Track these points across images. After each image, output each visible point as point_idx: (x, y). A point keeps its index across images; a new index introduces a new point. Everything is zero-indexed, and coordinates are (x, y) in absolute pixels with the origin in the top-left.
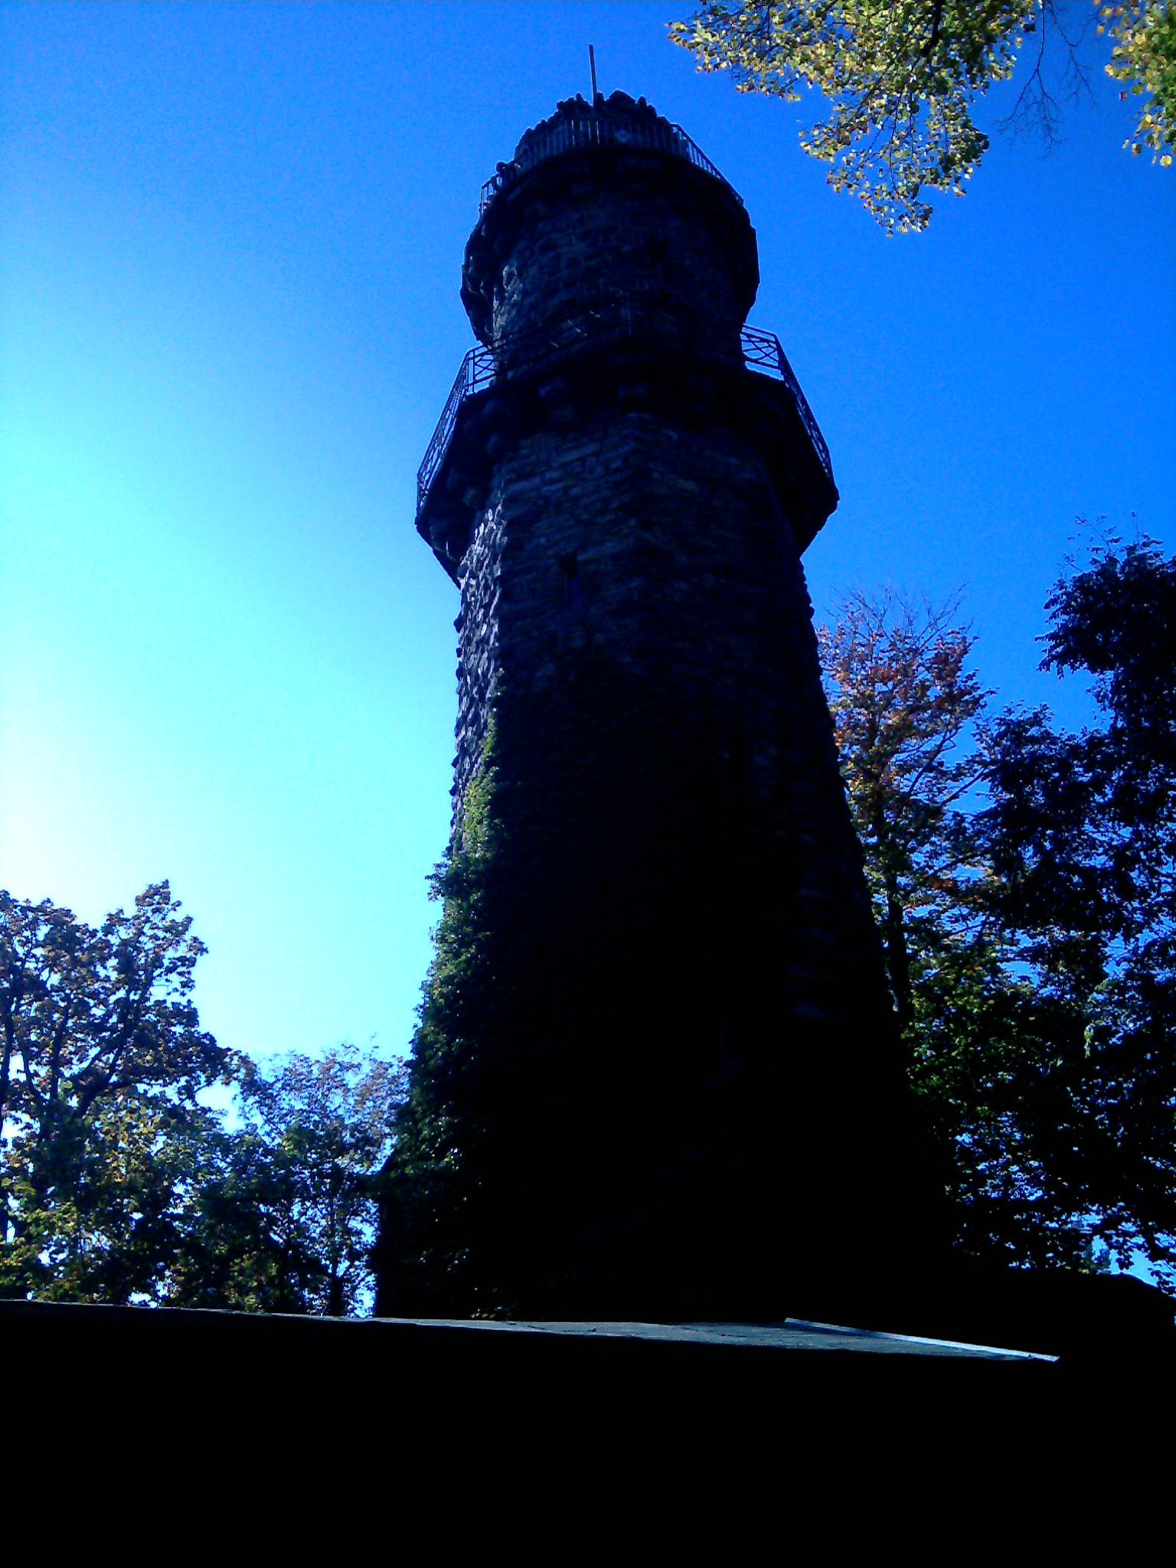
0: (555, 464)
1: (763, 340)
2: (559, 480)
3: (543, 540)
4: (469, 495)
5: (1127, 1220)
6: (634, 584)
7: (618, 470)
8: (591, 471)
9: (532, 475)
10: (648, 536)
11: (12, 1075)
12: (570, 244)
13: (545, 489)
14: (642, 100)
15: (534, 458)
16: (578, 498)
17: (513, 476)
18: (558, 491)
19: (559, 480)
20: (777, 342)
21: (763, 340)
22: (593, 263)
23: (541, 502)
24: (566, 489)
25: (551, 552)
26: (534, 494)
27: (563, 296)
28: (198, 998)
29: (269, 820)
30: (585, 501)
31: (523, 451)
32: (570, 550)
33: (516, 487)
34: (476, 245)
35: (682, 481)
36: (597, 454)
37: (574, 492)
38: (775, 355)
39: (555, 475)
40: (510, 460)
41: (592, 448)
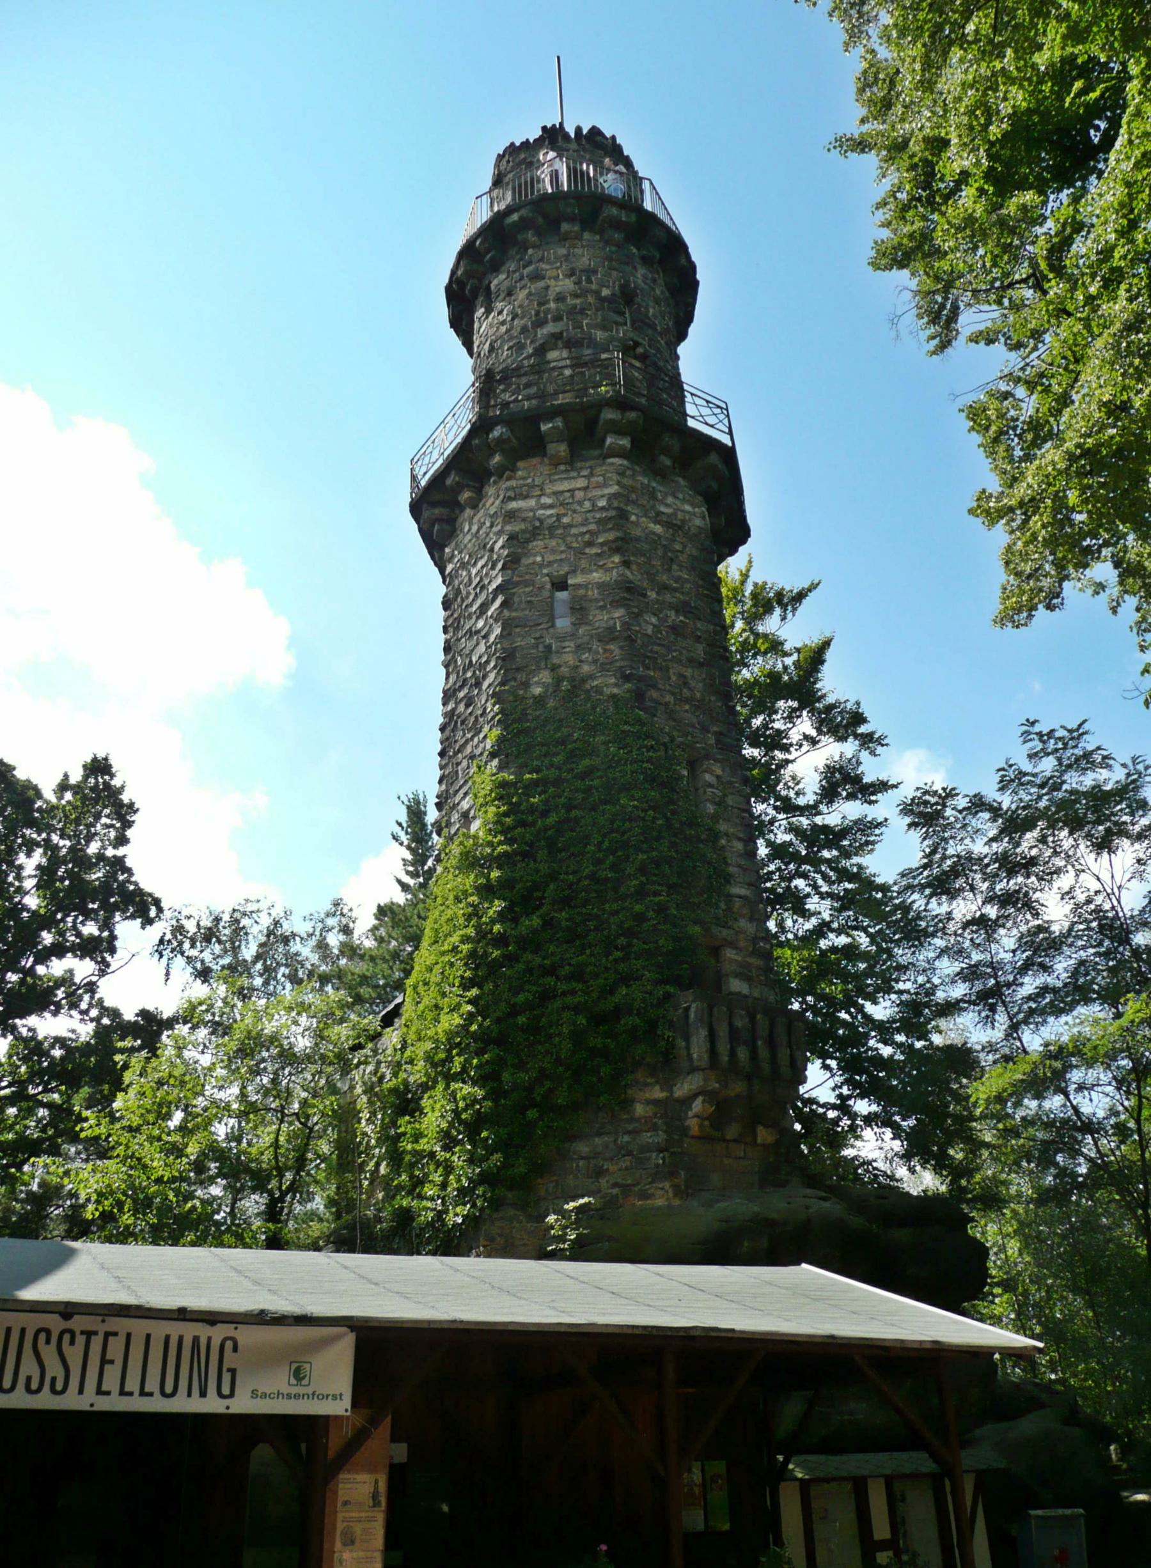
0: (548, 491)
1: (718, 407)
2: (551, 506)
3: (539, 559)
4: (466, 495)
5: (899, 1032)
6: (617, 615)
7: (602, 509)
8: (580, 503)
9: (526, 497)
10: (628, 573)
11: (9, 974)
12: (556, 278)
13: (541, 512)
14: (614, 138)
15: (530, 480)
16: (570, 526)
17: (511, 494)
18: (551, 516)
19: (551, 506)
20: (727, 410)
21: (718, 407)
22: (578, 301)
23: (537, 524)
24: (559, 517)
25: (545, 571)
26: (531, 514)
27: (550, 328)
28: (132, 854)
29: (282, 766)
30: (574, 531)
31: (520, 473)
32: (561, 573)
33: (514, 505)
34: (468, 252)
35: (652, 525)
36: (586, 489)
37: (565, 520)
38: (726, 422)
39: (549, 501)
40: (508, 479)
41: (581, 483)
